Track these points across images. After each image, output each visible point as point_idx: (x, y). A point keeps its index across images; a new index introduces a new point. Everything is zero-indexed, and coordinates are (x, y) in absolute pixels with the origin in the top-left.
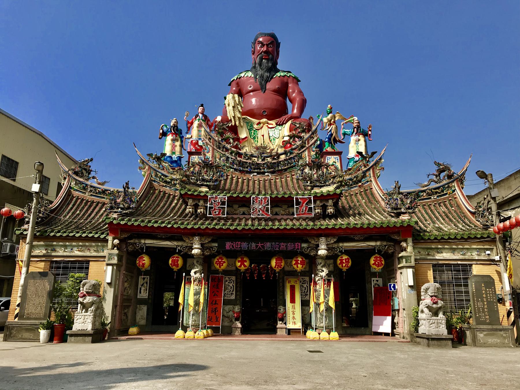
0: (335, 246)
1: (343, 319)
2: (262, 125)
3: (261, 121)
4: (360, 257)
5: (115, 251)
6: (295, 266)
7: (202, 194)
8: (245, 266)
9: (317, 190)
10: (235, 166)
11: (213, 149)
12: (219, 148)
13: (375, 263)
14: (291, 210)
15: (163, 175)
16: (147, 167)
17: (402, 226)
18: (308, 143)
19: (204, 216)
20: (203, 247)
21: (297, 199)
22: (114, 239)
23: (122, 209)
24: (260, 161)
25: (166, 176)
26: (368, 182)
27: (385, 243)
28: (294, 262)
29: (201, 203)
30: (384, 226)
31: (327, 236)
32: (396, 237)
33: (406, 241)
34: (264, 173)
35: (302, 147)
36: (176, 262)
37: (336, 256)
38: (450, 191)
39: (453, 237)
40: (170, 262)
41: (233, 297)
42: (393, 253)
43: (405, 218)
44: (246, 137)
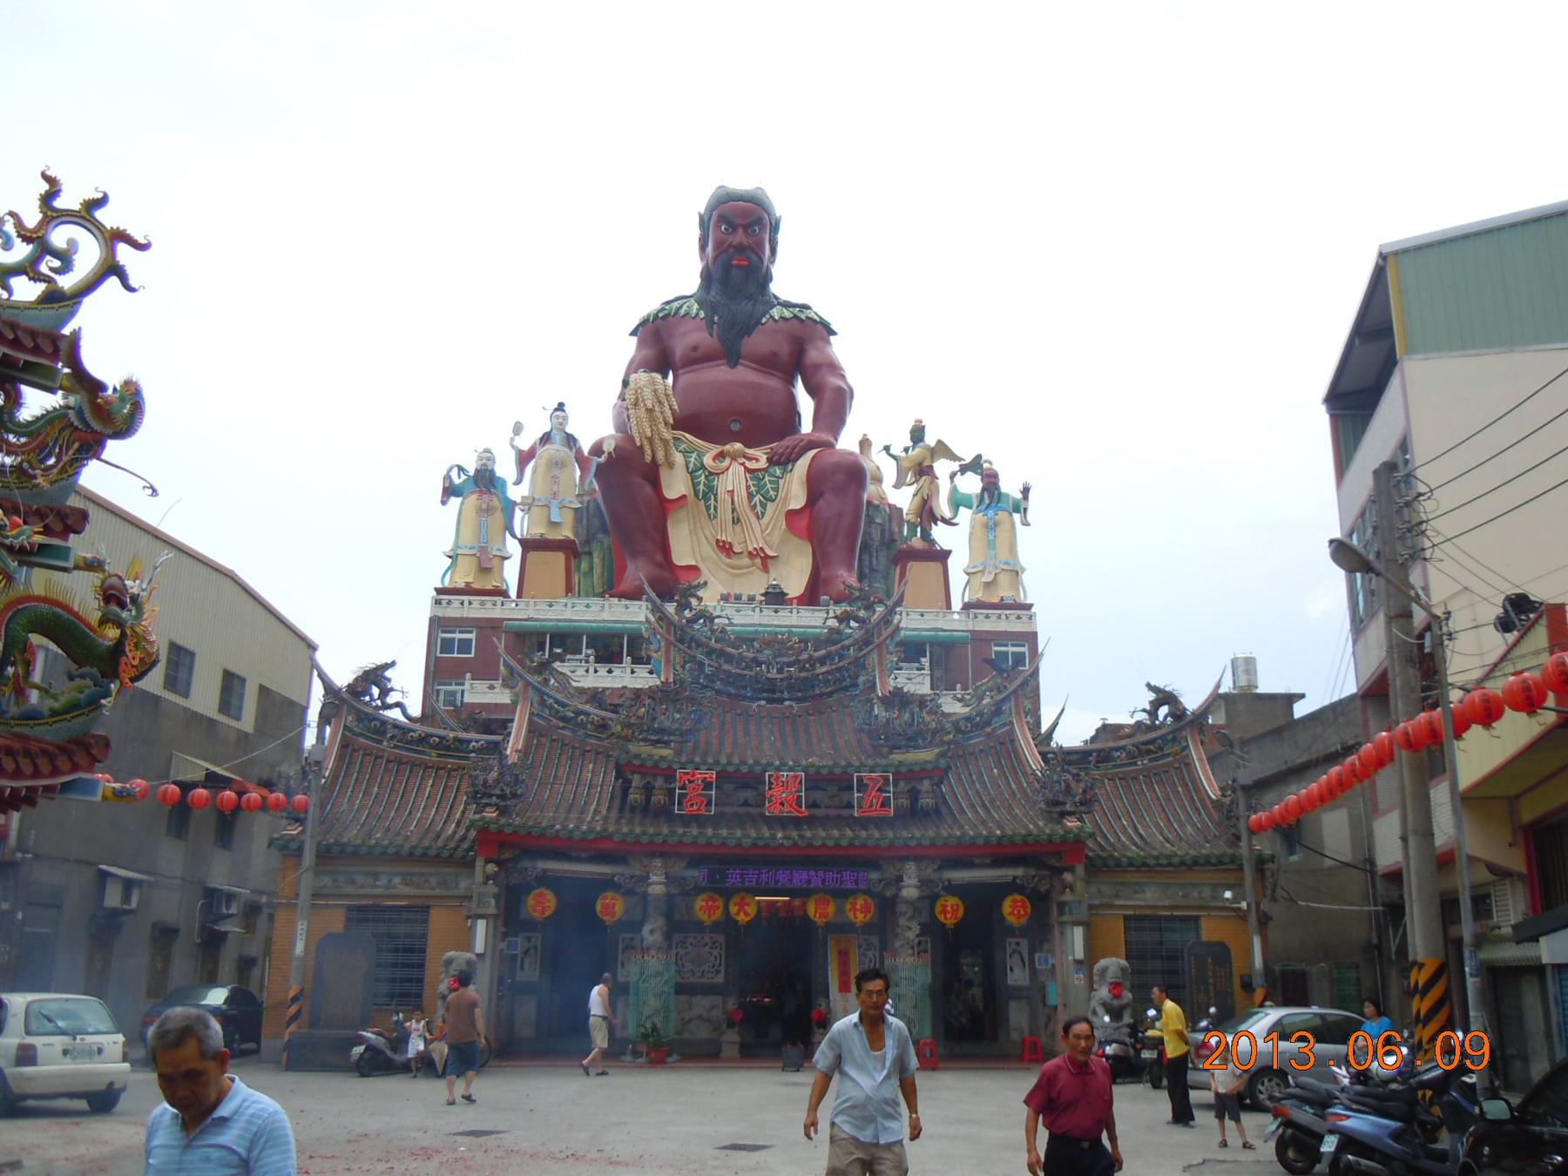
0: (935, 876)
1: (261, 893)
2: (728, 461)
3: (727, 447)
4: (982, 901)
5: (492, 888)
6: (851, 915)
7: (663, 765)
8: (746, 914)
9: (897, 757)
10: (718, 685)
11: (669, 643)
12: (681, 641)
13: (1012, 910)
14: (845, 797)
15: (557, 702)
16: (520, 684)
17: (1064, 842)
18: (880, 635)
19: (664, 813)
20: (670, 880)
21: (860, 779)
22: (488, 861)
23: (498, 797)
24: (773, 674)
25: (564, 705)
26: (1004, 725)
27: (1032, 872)
28: (848, 906)
29: (659, 782)
30: (1030, 840)
31: (917, 859)
32: (1053, 862)
33: (1072, 870)
34: (781, 701)
35: (867, 642)
36: (611, 907)
37: (934, 898)
38: (1177, 748)
39: (1164, 862)
40: (598, 908)
41: (720, 979)
42: (1048, 892)
43: (1071, 824)
44: (684, 497)
